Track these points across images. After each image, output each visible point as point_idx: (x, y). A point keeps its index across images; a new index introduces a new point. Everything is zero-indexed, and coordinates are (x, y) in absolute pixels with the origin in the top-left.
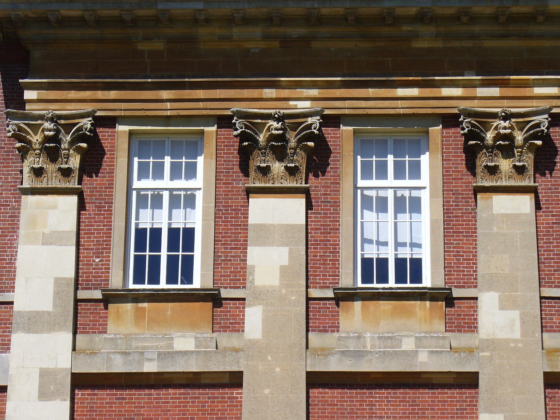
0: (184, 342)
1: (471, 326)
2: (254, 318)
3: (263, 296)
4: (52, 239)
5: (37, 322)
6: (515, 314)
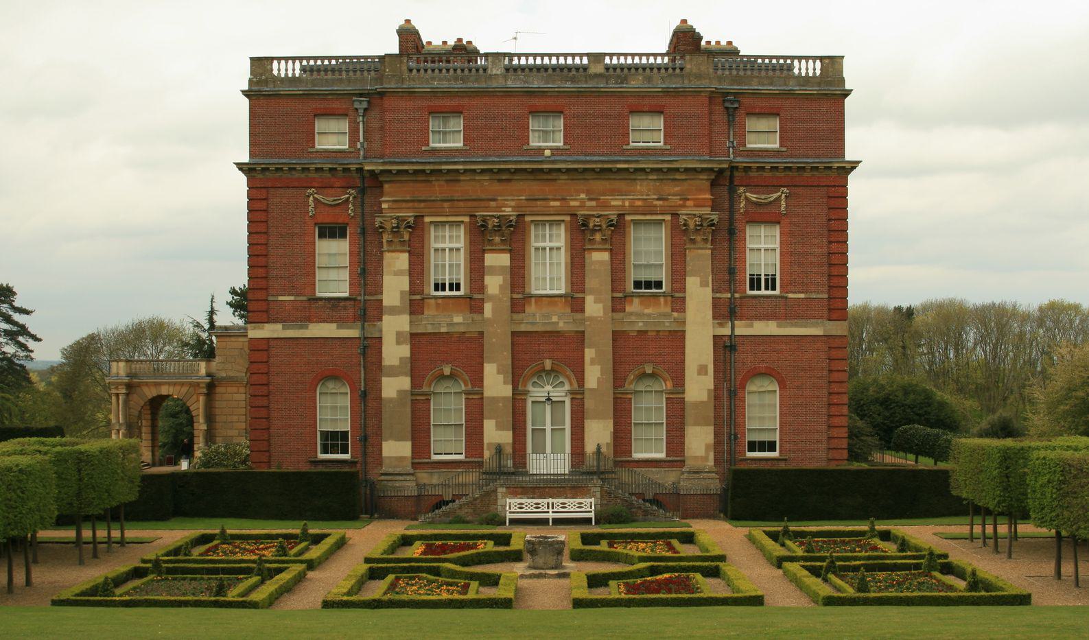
0: (458, 319)
1: (582, 310)
2: (488, 308)
3: (492, 298)
4: (398, 273)
5: (394, 311)
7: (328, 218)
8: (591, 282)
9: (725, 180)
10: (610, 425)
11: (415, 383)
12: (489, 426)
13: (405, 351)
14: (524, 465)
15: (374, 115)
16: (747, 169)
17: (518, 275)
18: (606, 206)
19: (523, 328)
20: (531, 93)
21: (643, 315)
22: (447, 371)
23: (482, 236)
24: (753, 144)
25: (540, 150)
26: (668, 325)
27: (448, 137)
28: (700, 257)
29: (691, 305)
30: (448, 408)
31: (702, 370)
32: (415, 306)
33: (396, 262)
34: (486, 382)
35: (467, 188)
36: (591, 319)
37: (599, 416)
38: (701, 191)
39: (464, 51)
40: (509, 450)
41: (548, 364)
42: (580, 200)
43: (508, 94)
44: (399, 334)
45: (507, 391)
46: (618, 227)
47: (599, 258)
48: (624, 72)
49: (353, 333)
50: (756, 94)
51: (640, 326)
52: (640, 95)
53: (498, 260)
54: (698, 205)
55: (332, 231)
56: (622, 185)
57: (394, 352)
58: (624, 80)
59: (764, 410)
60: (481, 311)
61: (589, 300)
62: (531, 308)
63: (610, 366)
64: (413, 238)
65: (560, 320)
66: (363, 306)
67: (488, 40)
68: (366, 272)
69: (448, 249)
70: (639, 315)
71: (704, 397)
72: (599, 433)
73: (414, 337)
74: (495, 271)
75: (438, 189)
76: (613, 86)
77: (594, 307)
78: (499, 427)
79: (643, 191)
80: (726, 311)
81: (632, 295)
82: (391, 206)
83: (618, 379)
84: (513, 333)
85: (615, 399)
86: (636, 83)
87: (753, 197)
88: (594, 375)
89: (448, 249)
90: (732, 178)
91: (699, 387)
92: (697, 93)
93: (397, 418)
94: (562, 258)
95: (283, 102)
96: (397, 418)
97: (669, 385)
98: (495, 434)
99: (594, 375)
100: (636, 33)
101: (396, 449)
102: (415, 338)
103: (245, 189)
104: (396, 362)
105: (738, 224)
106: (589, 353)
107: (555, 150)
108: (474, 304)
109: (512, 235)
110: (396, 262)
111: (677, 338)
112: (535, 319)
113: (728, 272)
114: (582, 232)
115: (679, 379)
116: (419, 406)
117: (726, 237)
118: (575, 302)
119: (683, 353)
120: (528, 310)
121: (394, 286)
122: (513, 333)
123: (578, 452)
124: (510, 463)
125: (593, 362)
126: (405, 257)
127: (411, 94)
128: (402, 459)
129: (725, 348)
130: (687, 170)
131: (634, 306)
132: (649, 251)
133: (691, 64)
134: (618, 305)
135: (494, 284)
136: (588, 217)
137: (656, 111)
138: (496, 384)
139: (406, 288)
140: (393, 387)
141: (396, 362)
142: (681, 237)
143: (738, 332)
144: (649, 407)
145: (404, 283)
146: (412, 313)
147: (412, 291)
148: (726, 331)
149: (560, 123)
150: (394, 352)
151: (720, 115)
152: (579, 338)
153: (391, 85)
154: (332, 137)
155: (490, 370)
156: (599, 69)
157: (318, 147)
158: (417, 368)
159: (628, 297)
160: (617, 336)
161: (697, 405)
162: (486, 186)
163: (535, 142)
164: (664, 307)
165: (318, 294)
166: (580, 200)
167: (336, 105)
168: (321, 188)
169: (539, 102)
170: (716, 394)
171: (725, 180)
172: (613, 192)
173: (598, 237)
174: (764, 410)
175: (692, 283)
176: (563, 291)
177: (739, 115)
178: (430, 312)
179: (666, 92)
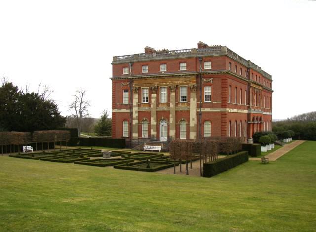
0: (146, 108)
2: (152, 106)
3: (153, 104)
4: (136, 99)
5: (135, 106)
7: (125, 88)
8: (171, 100)
9: (199, 76)
10: (175, 131)
11: (139, 121)
12: (152, 130)
13: (137, 115)
14: (159, 139)
15: (133, 67)
16: (203, 74)
17: (158, 99)
18: (174, 84)
19: (159, 110)
20: (160, 60)
21: (182, 107)
22: (183, 119)
23: (151, 91)
24: (206, 68)
25: (162, 72)
26: (186, 109)
27: (145, 70)
28: (193, 94)
29: (191, 105)
30: (145, 126)
31: (193, 119)
32: (139, 105)
33: (136, 96)
34: (151, 121)
35: (149, 81)
36: (172, 108)
37: (173, 129)
38: (194, 79)
39: (165, 52)
40: (155, 136)
41: (163, 118)
42: (169, 83)
43: (156, 61)
44: (136, 111)
45: (155, 123)
46: (177, 87)
47: (173, 95)
48: (178, 55)
49: (129, 111)
50: (206, 57)
51: (181, 110)
52: (181, 59)
53: (154, 96)
54: (193, 83)
55: (126, 91)
56: (177, 79)
57: (135, 115)
58: (178, 56)
59: (208, 129)
60: (150, 106)
61: (171, 104)
62: (160, 106)
63: (175, 118)
64: (139, 91)
65: (165, 108)
66: (130, 106)
67: (171, 48)
68: (131, 99)
69: (145, 93)
70: (181, 107)
71: (193, 125)
72: (172, 133)
73: (139, 112)
74: (153, 98)
75: (143, 81)
76: (176, 57)
77: (172, 106)
78: (154, 131)
79: (182, 80)
80: (199, 106)
81: (180, 103)
82: (135, 86)
83: (176, 121)
84: (157, 111)
85: (176, 126)
86: (181, 57)
87: (205, 80)
88: (172, 120)
89: (145, 93)
90: (201, 76)
91: (193, 123)
92: (193, 57)
93: (135, 128)
94: (166, 95)
95: (118, 64)
96: (135, 128)
97: (187, 122)
98: (153, 132)
99: (172, 120)
100: (188, 44)
101: (135, 135)
102: (139, 112)
103: (111, 83)
105: (203, 86)
106: (171, 115)
107: (165, 72)
108: (149, 105)
109: (156, 90)
110: (136, 96)
111: (188, 112)
112: (161, 108)
113: (200, 98)
114: (170, 89)
115: (188, 121)
116: (140, 126)
117: (199, 89)
118: (168, 104)
119: (189, 115)
120: (179, 106)
121: (135, 101)
122: (157, 111)
123: (169, 137)
124: (156, 139)
125: (171, 117)
126: (137, 95)
127: (139, 62)
128: (136, 137)
129: (199, 114)
130: (189, 75)
131: (180, 105)
132: (184, 92)
133: (203, 50)
134: (177, 105)
135: (153, 101)
136: (170, 86)
137: (184, 62)
138: (153, 122)
139: (137, 102)
140: (135, 122)
142: (189, 90)
143: (202, 111)
144: (183, 127)
145: (137, 101)
146: (138, 107)
147: (138, 103)
148: (199, 111)
149: (166, 66)
150: (135, 115)
151: (198, 62)
152: (168, 113)
153: (135, 61)
154: (126, 72)
155: (152, 119)
156: (174, 54)
157: (124, 74)
158: (139, 118)
159: (179, 103)
160: (176, 111)
161: (192, 127)
162: (152, 80)
163: (162, 71)
164: (186, 105)
165: (124, 103)
166: (169, 83)
167: (145, 63)
168: (124, 82)
169: (162, 62)
170: (197, 125)
171: (199, 76)
172: (176, 80)
173: (173, 90)
174: (208, 129)
175: (191, 100)
176: (166, 102)
177: (203, 62)
178: (142, 107)
179: (186, 58)
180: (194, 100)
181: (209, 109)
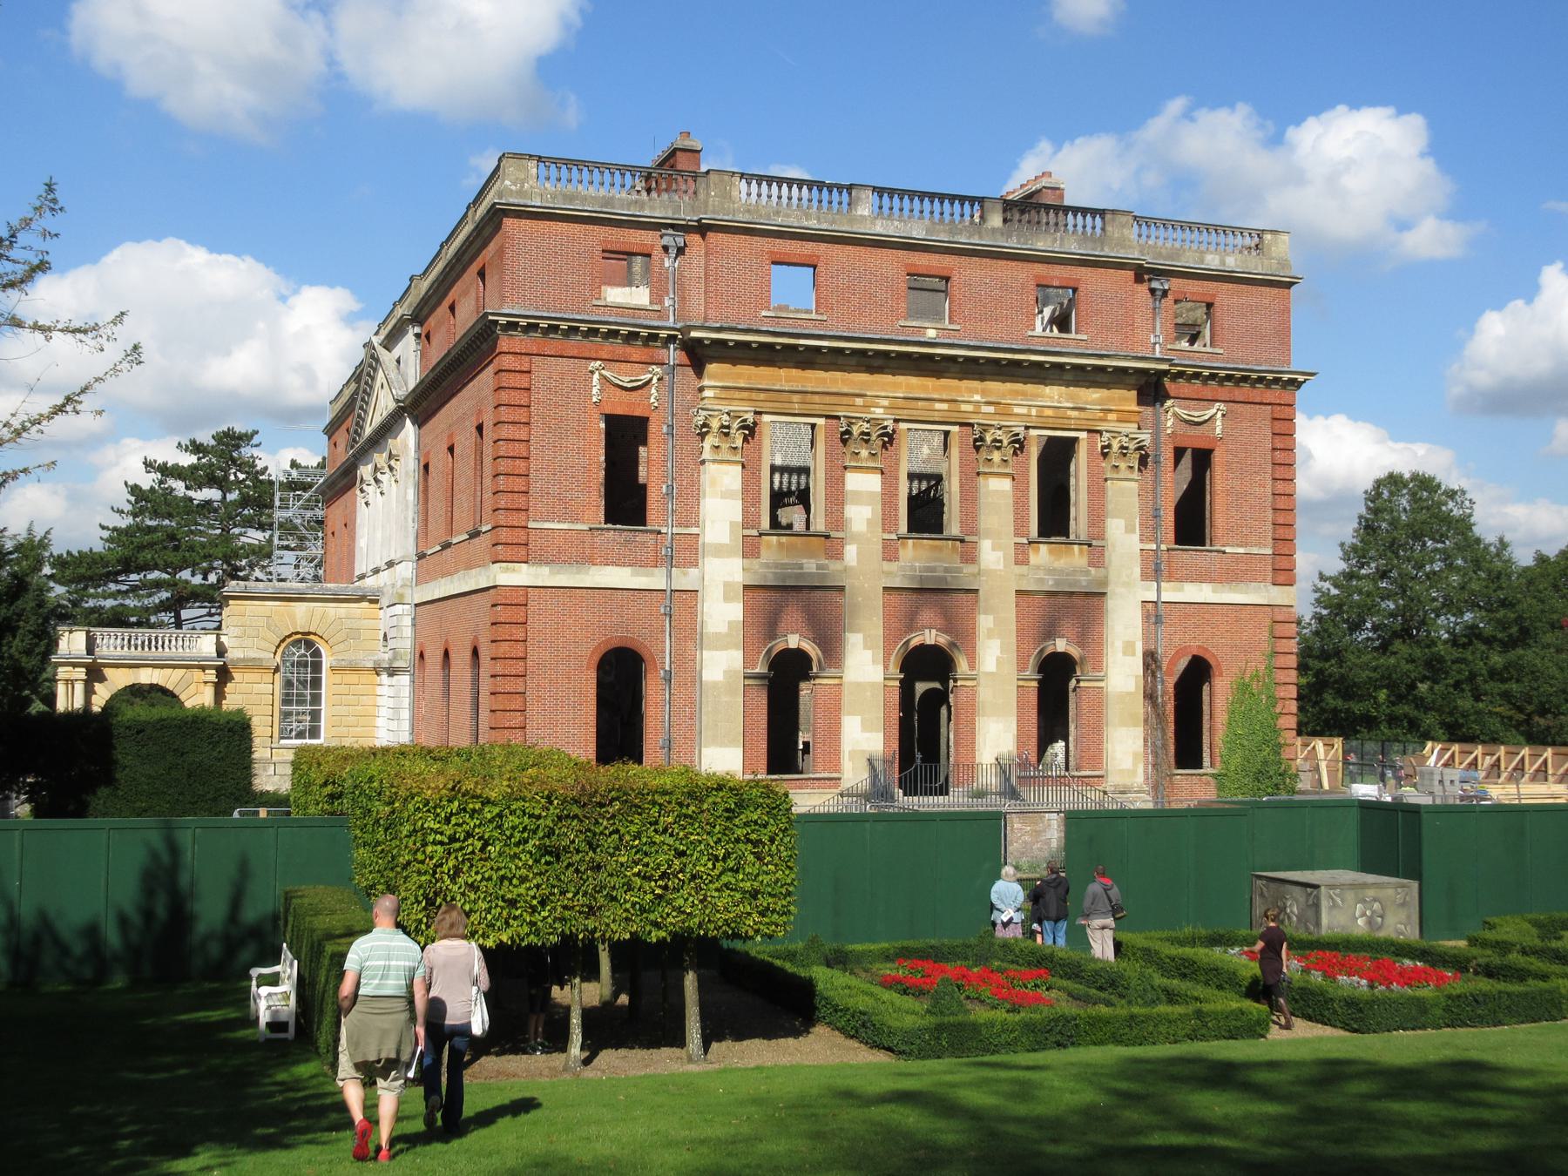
4: (726, 495)
5: (719, 551)
6: (1000, 554)
104: (723, 629)
141: (723, 629)
180: (1129, 529)
181: (545, 570)
